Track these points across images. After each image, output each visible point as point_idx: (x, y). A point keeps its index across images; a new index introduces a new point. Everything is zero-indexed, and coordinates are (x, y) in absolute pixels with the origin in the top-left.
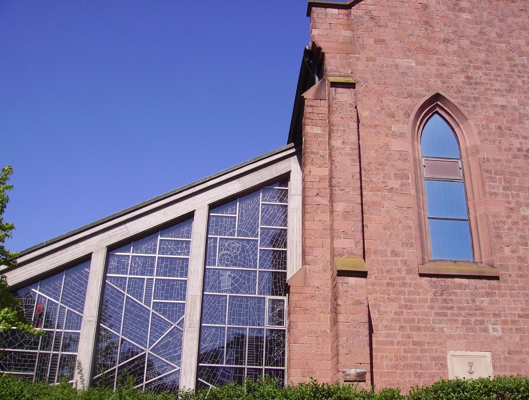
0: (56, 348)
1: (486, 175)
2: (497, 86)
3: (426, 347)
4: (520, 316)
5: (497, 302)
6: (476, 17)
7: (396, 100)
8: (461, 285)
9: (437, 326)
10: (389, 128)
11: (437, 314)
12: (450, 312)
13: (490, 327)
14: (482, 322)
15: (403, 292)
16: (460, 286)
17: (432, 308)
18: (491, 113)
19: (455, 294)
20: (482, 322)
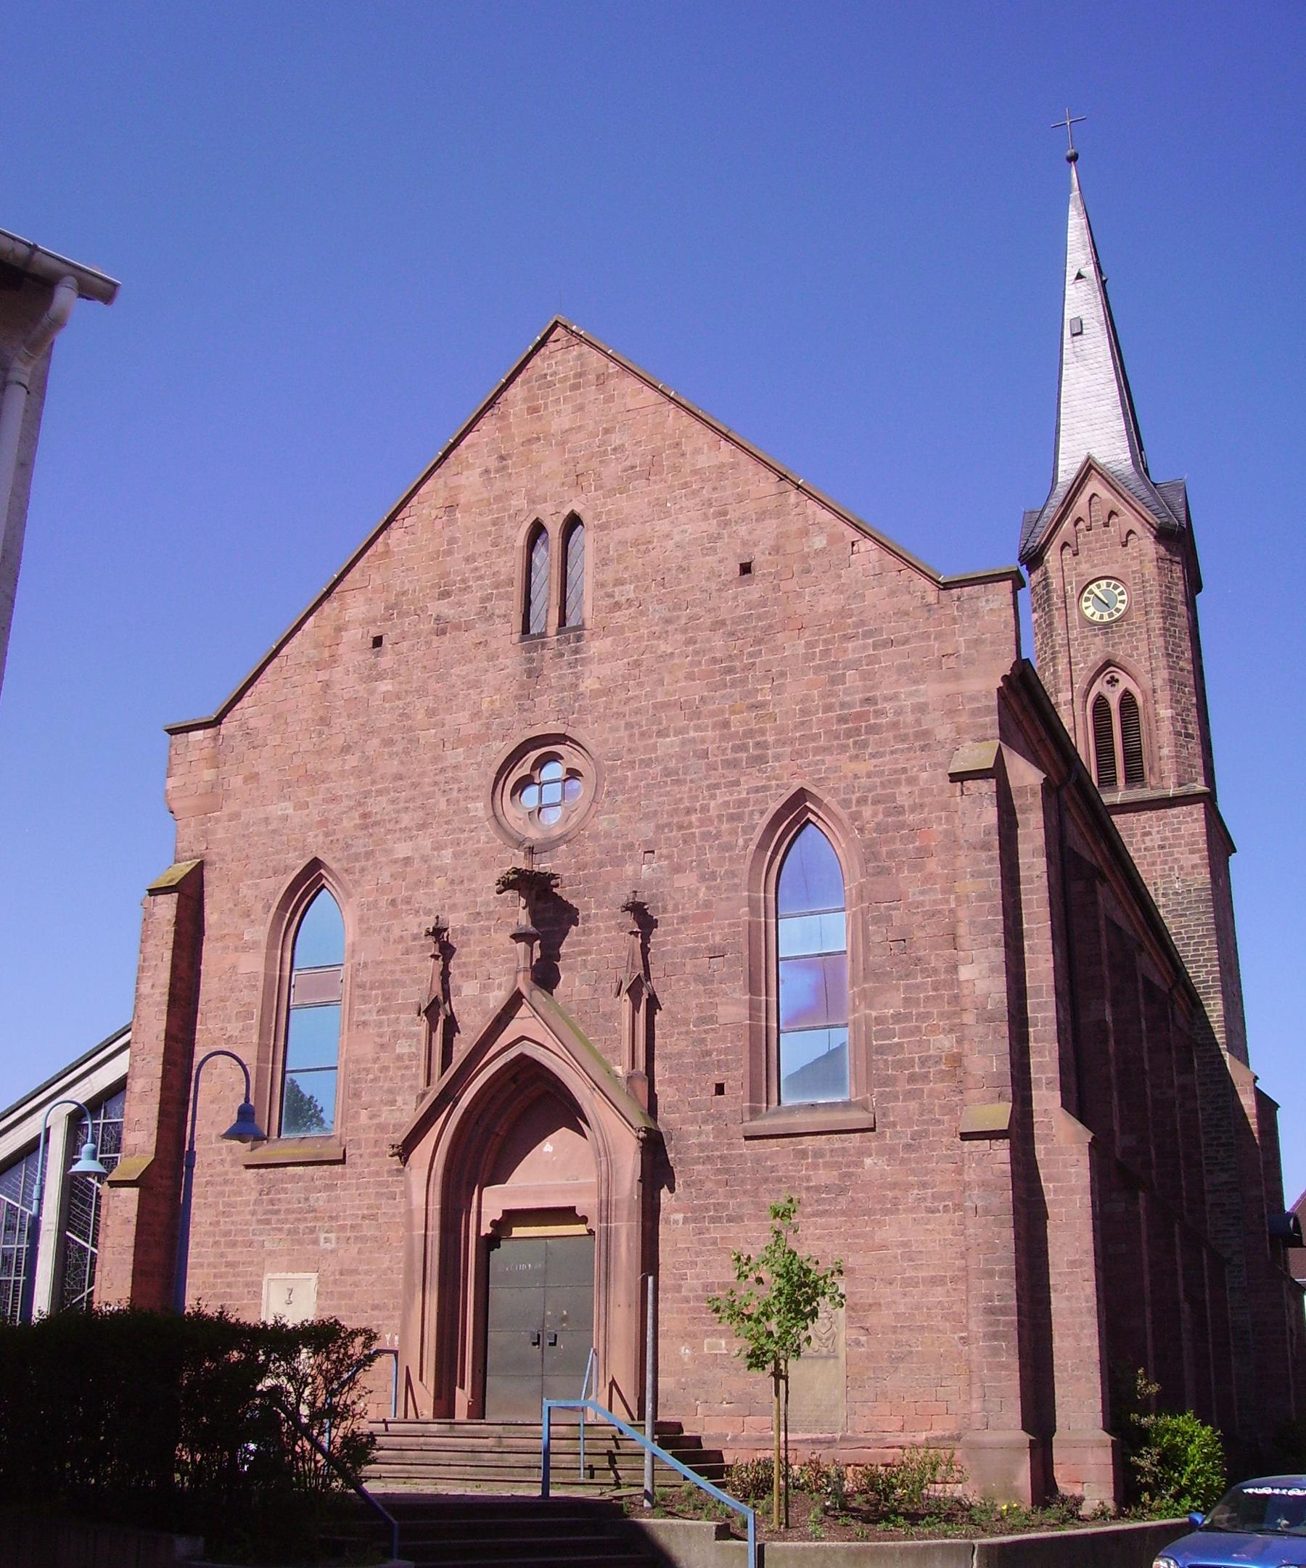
0: (16, 1282)
1: (358, 992)
2: (406, 820)
3: (241, 1268)
4: (364, 1217)
5: (338, 1198)
6: (401, 683)
7: (256, 885)
8: (294, 1176)
9: (256, 1238)
10: (240, 936)
11: (260, 1222)
12: (274, 1218)
13: (322, 1236)
14: (312, 1230)
15: (222, 1194)
16: (294, 1179)
17: (253, 1213)
18: (385, 877)
19: (285, 1191)
20: (312, 1230)
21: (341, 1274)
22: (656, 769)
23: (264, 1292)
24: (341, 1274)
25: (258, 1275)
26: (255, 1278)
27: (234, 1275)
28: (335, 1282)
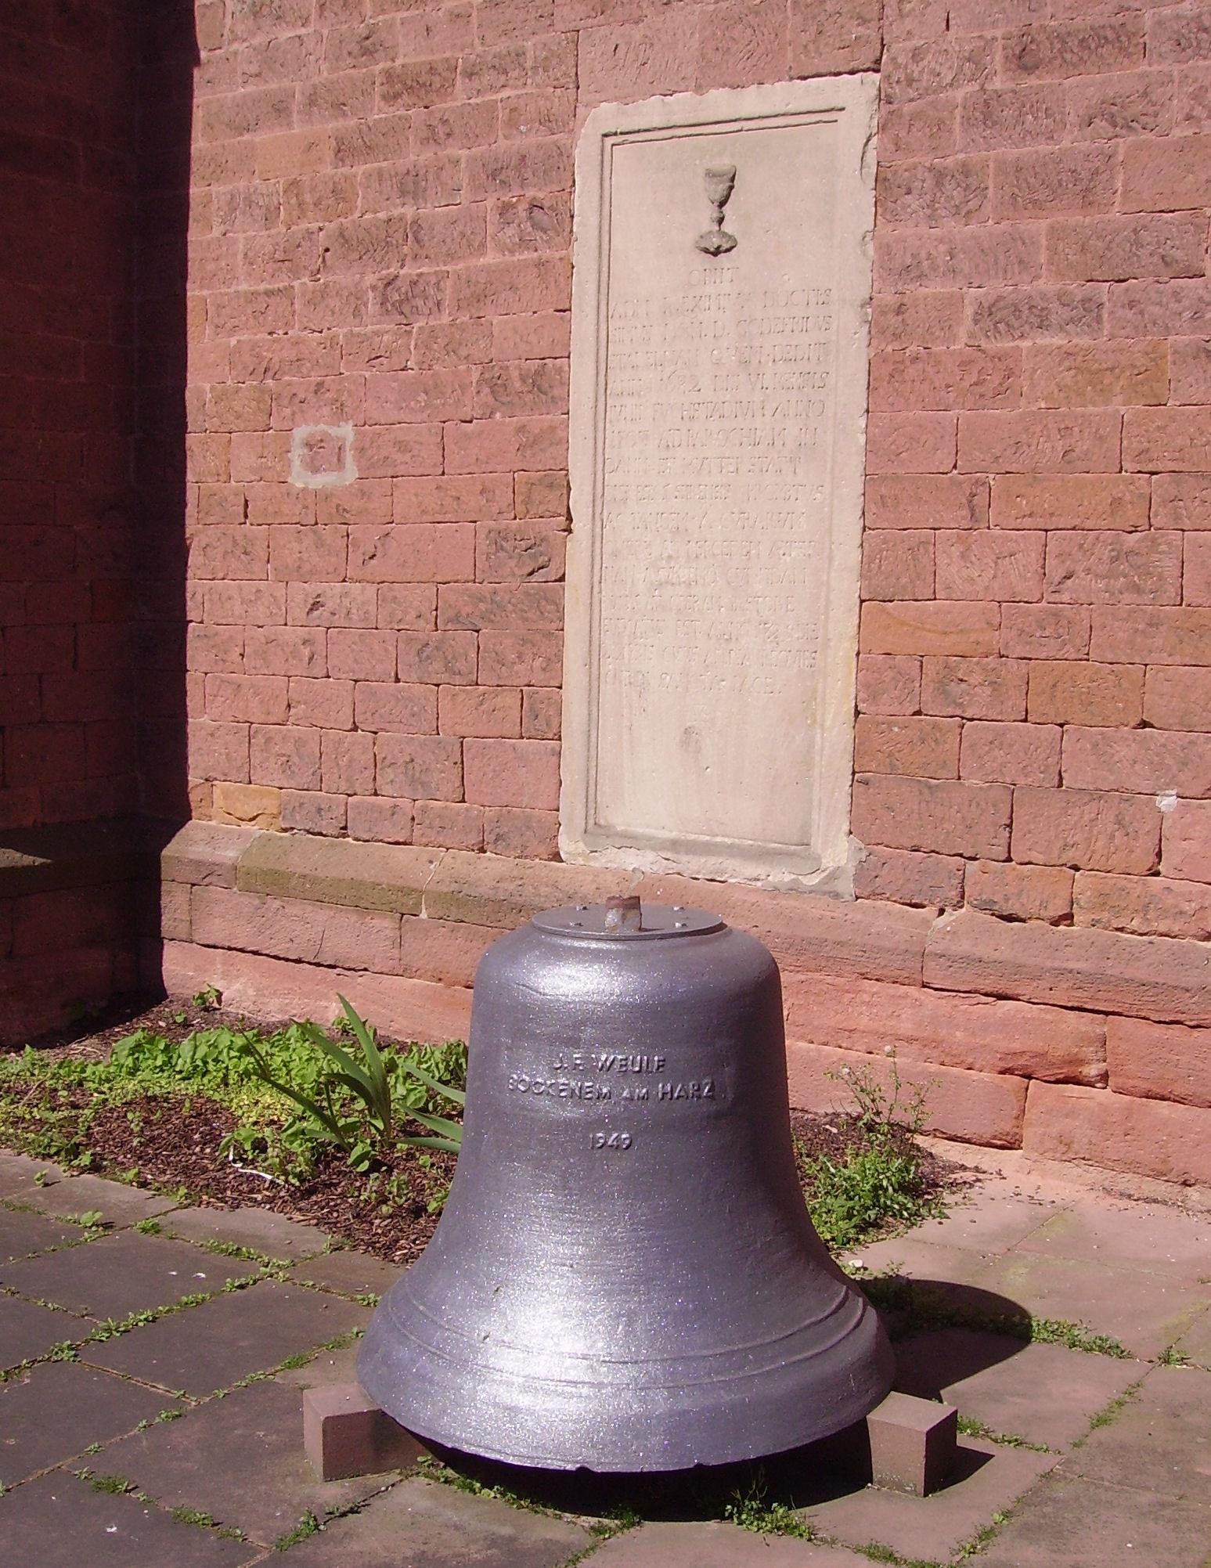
3: (460, 97)
21: (1023, 60)
22: (367, 445)
23: (584, 202)
24: (1023, 60)
25: (546, 121)
26: (529, 140)
27: (431, 137)
28: (986, 113)
